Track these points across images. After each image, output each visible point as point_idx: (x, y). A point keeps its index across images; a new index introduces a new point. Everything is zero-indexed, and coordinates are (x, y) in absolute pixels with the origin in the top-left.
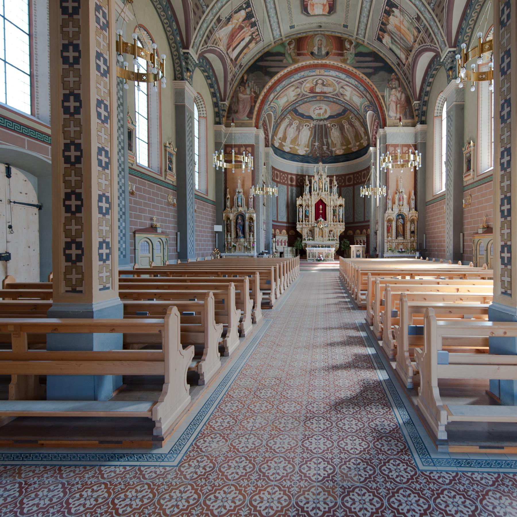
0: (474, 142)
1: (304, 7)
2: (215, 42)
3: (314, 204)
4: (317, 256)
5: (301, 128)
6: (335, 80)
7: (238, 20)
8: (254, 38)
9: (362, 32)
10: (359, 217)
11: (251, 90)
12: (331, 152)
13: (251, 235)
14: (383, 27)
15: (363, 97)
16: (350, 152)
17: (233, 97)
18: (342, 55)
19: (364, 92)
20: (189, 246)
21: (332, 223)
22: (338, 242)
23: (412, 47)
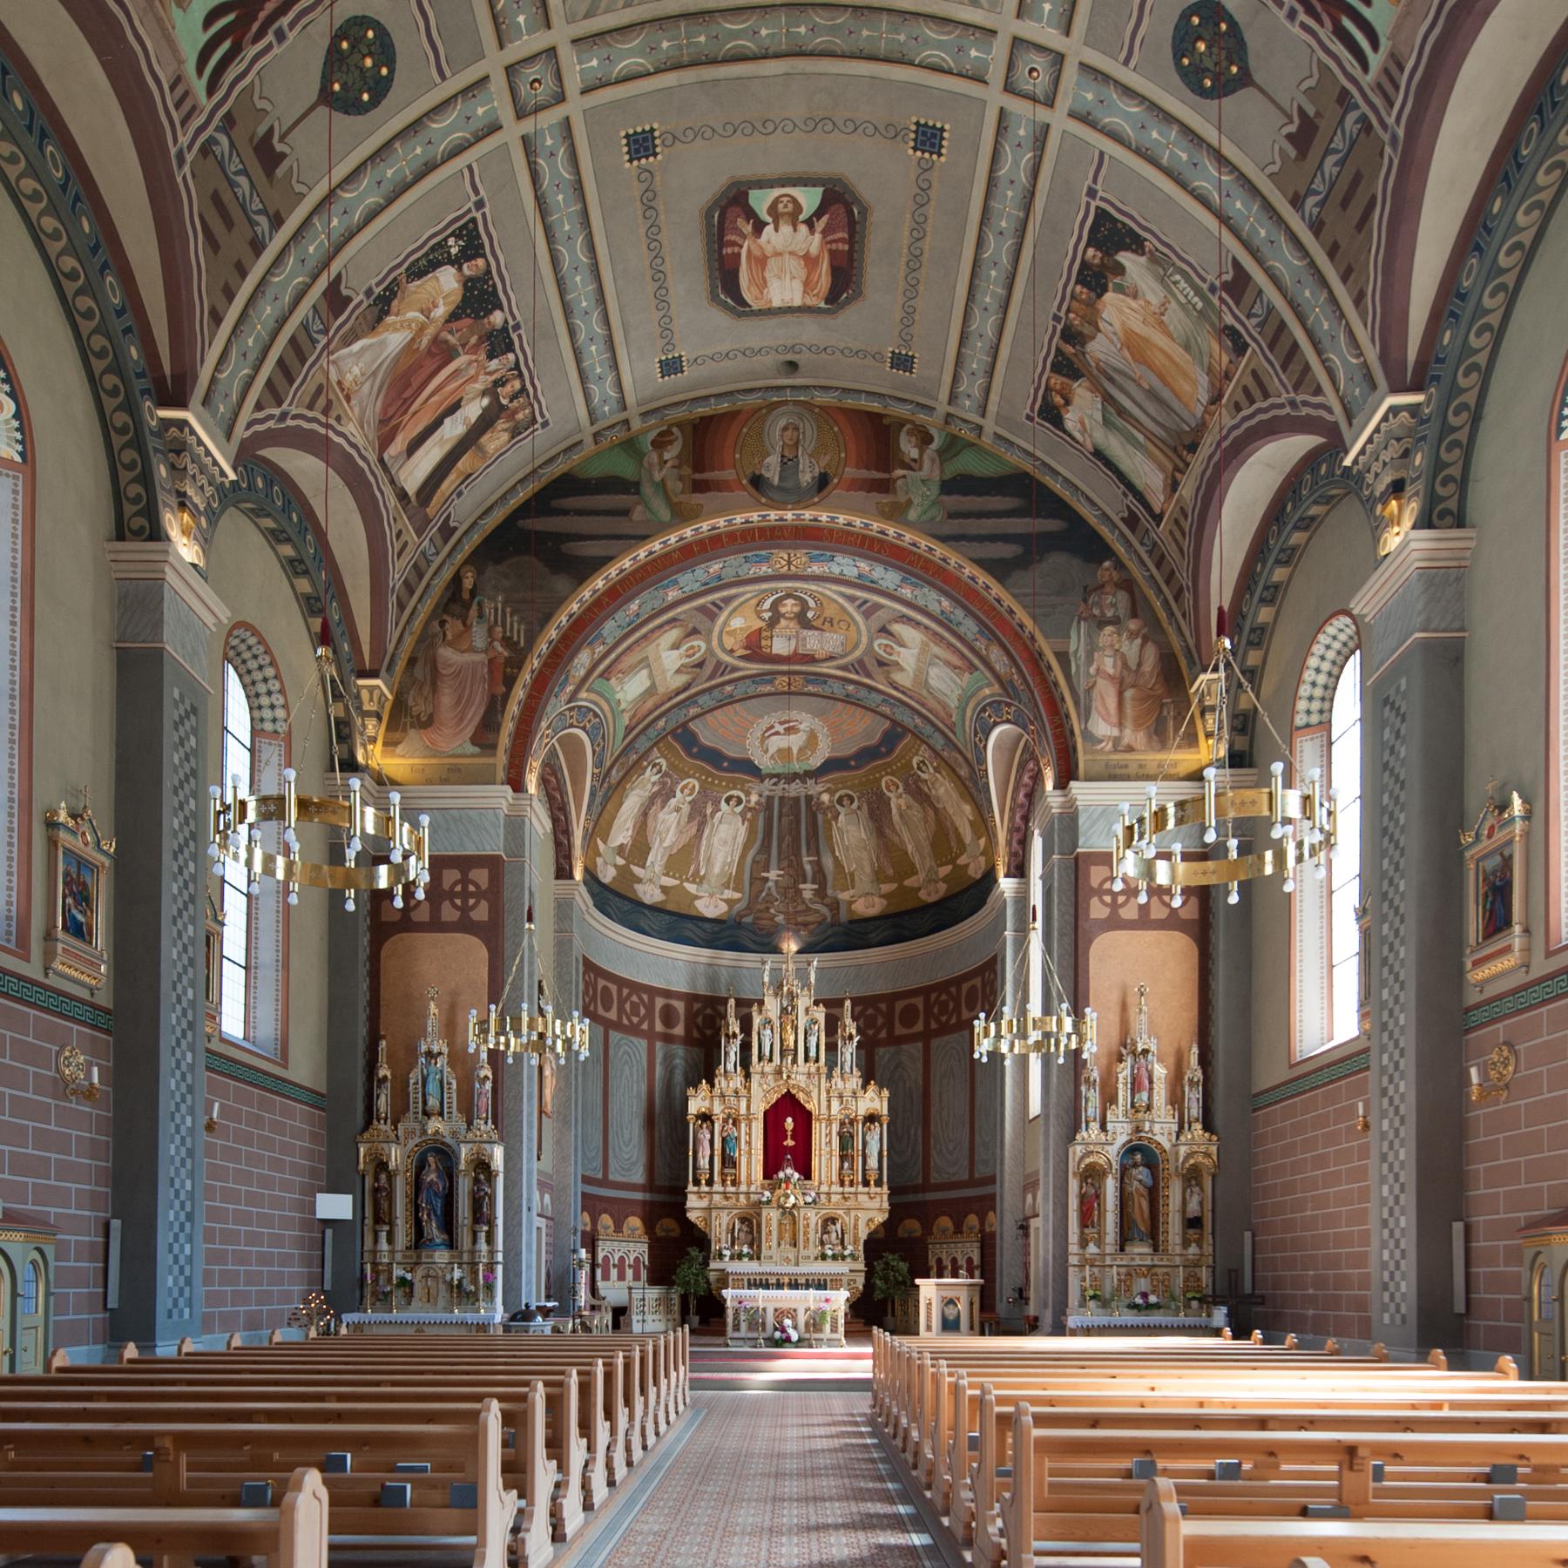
0: (1526, 800)
1: (721, 268)
2: (322, 402)
3: (759, 1107)
4: (770, 1319)
5: (709, 811)
6: (852, 599)
7: (426, 312)
8: (502, 408)
9: (971, 387)
10: (948, 1165)
11: (490, 631)
12: (835, 906)
13: (482, 1236)
14: (1069, 349)
15: (972, 668)
16: (911, 905)
17: (412, 662)
18: (885, 487)
19: (980, 645)
20: (167, 1280)
21: (836, 1188)
22: (861, 1265)
23: (1202, 427)
